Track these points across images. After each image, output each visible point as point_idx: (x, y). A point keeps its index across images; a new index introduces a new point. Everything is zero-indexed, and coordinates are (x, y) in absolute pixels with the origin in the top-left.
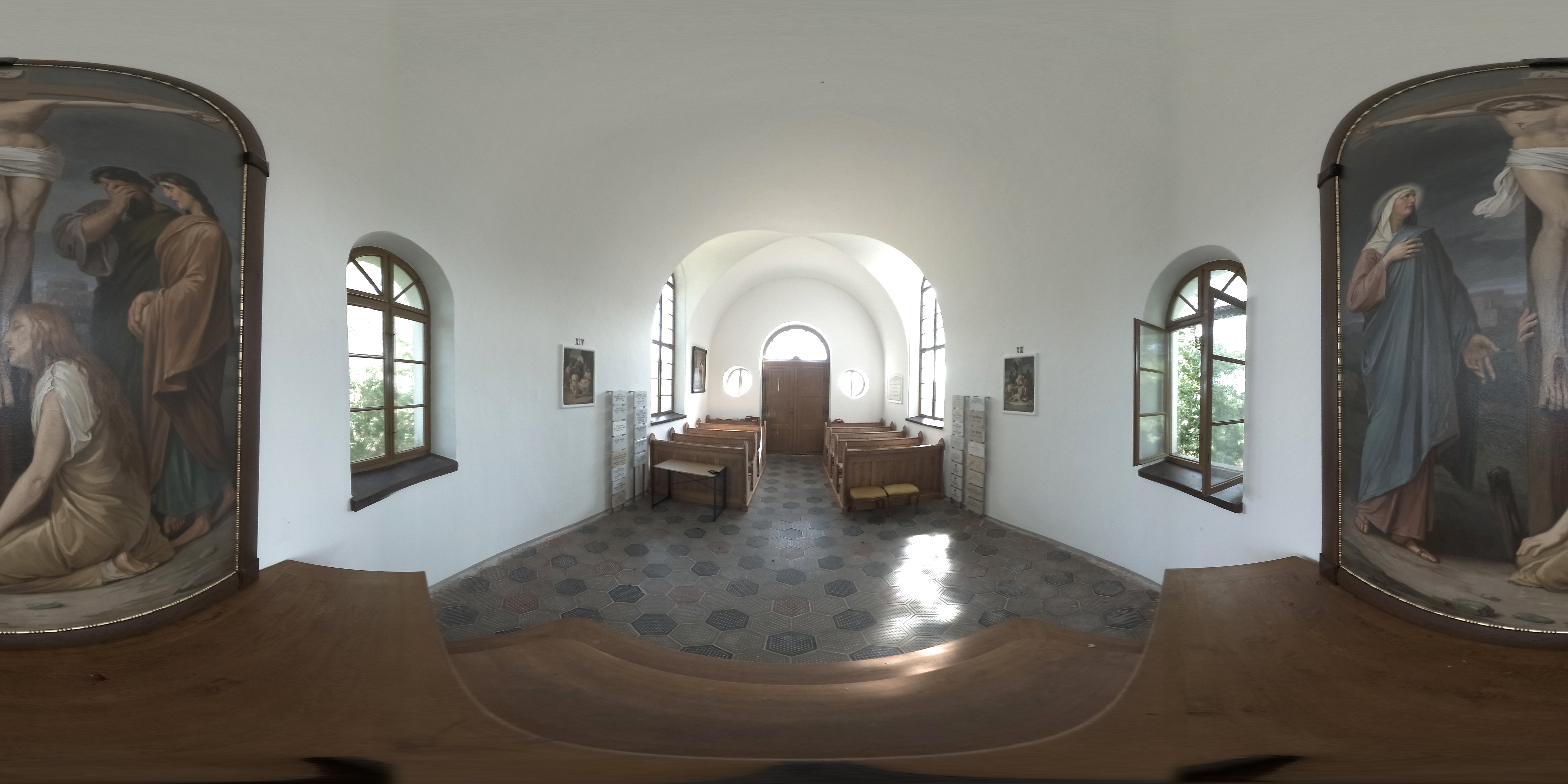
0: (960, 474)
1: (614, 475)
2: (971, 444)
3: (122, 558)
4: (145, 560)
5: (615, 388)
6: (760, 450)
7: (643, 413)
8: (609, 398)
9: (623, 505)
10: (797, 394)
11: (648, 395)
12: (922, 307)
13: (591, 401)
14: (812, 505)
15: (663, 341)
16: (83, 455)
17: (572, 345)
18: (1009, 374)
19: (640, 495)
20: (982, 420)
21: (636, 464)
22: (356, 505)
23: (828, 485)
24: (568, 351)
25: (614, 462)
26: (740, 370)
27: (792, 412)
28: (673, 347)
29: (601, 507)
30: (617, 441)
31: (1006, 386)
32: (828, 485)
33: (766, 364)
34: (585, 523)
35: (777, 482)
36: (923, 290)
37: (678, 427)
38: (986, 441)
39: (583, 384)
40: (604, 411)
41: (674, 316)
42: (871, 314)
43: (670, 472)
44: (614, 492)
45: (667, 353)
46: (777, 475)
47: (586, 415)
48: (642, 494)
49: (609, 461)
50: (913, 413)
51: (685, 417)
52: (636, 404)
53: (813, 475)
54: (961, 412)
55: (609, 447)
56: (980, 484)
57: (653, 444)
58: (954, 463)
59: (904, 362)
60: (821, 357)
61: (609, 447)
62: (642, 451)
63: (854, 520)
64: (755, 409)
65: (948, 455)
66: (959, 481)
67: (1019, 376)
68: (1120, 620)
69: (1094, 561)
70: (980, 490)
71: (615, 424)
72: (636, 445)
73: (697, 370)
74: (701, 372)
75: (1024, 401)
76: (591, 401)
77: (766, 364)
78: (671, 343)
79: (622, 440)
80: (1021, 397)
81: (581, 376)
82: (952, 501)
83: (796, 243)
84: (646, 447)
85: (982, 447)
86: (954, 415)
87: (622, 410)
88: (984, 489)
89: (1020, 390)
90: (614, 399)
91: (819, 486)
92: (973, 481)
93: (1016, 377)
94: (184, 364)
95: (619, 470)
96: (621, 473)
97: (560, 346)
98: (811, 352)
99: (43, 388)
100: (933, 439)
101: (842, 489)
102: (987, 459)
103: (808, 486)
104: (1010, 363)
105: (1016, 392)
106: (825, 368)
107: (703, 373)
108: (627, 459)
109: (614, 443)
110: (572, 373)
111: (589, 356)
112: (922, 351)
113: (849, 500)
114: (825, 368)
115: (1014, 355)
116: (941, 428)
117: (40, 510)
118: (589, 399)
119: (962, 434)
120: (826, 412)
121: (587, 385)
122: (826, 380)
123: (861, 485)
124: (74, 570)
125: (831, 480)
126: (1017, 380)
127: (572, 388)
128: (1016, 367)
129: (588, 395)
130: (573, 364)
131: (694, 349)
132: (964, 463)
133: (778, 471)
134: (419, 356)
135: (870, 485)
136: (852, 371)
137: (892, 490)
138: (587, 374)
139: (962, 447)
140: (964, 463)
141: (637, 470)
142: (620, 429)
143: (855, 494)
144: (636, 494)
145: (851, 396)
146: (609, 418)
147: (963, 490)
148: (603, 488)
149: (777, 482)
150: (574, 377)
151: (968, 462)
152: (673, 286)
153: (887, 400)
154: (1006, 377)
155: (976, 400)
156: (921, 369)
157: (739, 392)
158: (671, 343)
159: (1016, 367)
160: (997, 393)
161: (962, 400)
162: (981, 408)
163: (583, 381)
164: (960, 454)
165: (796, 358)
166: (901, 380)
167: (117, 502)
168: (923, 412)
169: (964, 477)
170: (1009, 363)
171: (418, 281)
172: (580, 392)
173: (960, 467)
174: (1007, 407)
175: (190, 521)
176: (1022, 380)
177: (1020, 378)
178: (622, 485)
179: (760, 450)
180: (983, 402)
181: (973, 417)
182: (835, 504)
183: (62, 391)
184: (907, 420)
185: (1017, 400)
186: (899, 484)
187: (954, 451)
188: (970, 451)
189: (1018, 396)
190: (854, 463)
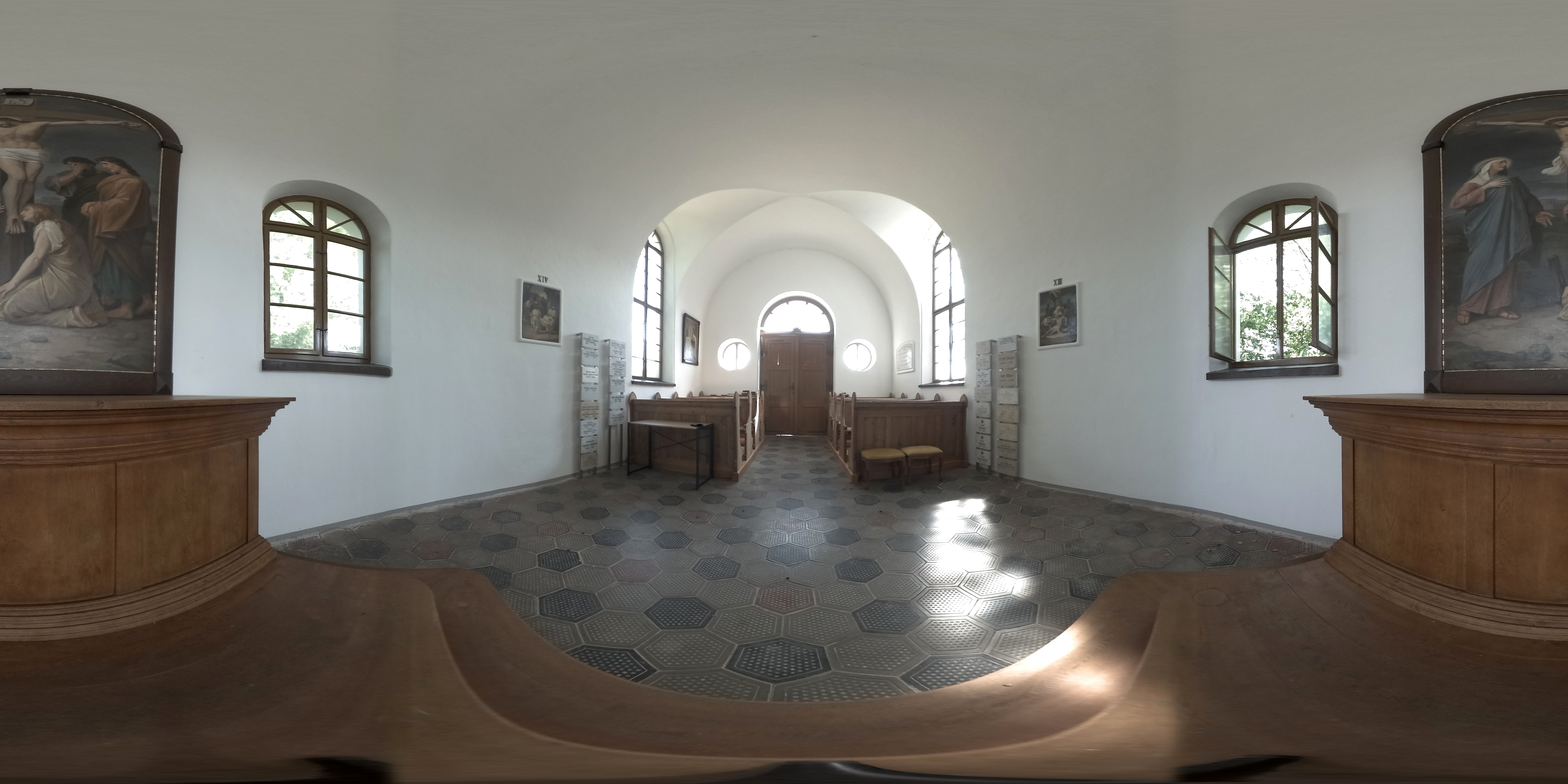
0: (988, 431)
1: (583, 429)
2: (1001, 392)
3: (77, 309)
4: (91, 317)
5: (587, 331)
6: (757, 418)
7: (621, 368)
8: (578, 341)
9: (595, 469)
10: (799, 364)
11: (627, 347)
12: (934, 269)
13: (557, 341)
14: (816, 476)
15: (649, 303)
16: (58, 251)
17: (534, 281)
18: (1045, 307)
19: (616, 464)
20: (1014, 361)
21: (611, 422)
22: (294, 399)
23: (834, 458)
24: (528, 287)
25: (583, 412)
26: (737, 344)
27: (793, 388)
28: (661, 312)
29: (568, 469)
30: (587, 389)
31: (1041, 319)
32: (834, 458)
33: (764, 336)
34: (547, 485)
35: (776, 456)
36: (935, 254)
37: (666, 394)
38: (1020, 384)
39: (546, 320)
40: (572, 354)
41: (662, 281)
42: (879, 282)
43: (650, 427)
44: (583, 450)
45: (654, 318)
46: (777, 450)
47: (549, 357)
48: (620, 463)
49: (579, 411)
50: (926, 380)
51: (675, 385)
52: (612, 353)
53: (816, 450)
54: (988, 358)
55: (578, 397)
56: (1013, 437)
57: (634, 404)
58: (980, 420)
59: (916, 327)
60: (826, 329)
61: (578, 397)
62: (619, 409)
63: (867, 489)
64: (753, 383)
65: (971, 416)
66: (987, 440)
67: (1058, 308)
68: (1216, 557)
69: (1158, 509)
70: (1013, 445)
71: (585, 369)
72: (612, 400)
73: (688, 339)
74: (693, 343)
75: (1064, 332)
76: (557, 341)
77: (764, 336)
78: (659, 307)
79: (594, 389)
80: (1061, 329)
81: (544, 313)
82: (978, 467)
83: (798, 211)
84: (623, 404)
85: (1014, 392)
86: (978, 363)
87: (595, 356)
88: (1018, 442)
89: (1059, 321)
90: (584, 342)
91: (824, 459)
92: (1004, 436)
93: (1054, 309)
94: (115, 228)
95: (589, 424)
96: (593, 429)
97: (519, 281)
98: (814, 324)
99: (39, 228)
100: (953, 396)
101: (851, 459)
102: (1020, 405)
103: (811, 459)
104: (1045, 297)
105: (1055, 324)
106: (829, 338)
107: (695, 345)
108: (600, 412)
109: (583, 391)
110: (533, 307)
111: (554, 296)
112: (935, 313)
113: (860, 464)
114: (829, 338)
115: (1050, 287)
116: (962, 385)
117: (37, 272)
118: (553, 337)
119: (989, 383)
120: (830, 387)
121: (552, 323)
122: (830, 353)
123: (873, 447)
124: (54, 310)
125: (838, 453)
126: (1055, 312)
127: (533, 323)
128: (1054, 299)
129: (552, 333)
130: (535, 299)
131: (685, 316)
132: (992, 417)
133: (777, 448)
134: (359, 308)
135: (884, 447)
136: (858, 344)
137: (911, 451)
138: (552, 312)
139: (989, 398)
140: (992, 417)
141: (613, 431)
142: (592, 374)
143: (867, 455)
144: (612, 462)
145: (857, 366)
146: (578, 363)
147: (992, 450)
148: (571, 445)
149: (776, 456)
150: (535, 312)
151: (998, 414)
152: (661, 253)
153: (896, 372)
154: (1041, 311)
155: (1005, 340)
156: (934, 331)
157: (736, 364)
158: (659, 307)
159: (1054, 299)
160: (1032, 331)
161: (988, 345)
162: (1013, 347)
163: (546, 317)
164: (987, 406)
165: (797, 330)
166: (913, 346)
167: (75, 275)
168: (937, 378)
169: (992, 434)
170: (1045, 297)
171: (355, 218)
172: (544, 328)
173: (987, 422)
174: (1044, 341)
175: (117, 305)
176: (1062, 310)
177: (1058, 310)
178: (593, 444)
179: (757, 418)
180: (1015, 340)
181: (1002, 361)
182: (843, 474)
183: (48, 229)
184: (921, 386)
185: (1056, 333)
186: (915, 451)
187: (980, 404)
188: (1000, 399)
189: (1056, 328)
190: (866, 418)
